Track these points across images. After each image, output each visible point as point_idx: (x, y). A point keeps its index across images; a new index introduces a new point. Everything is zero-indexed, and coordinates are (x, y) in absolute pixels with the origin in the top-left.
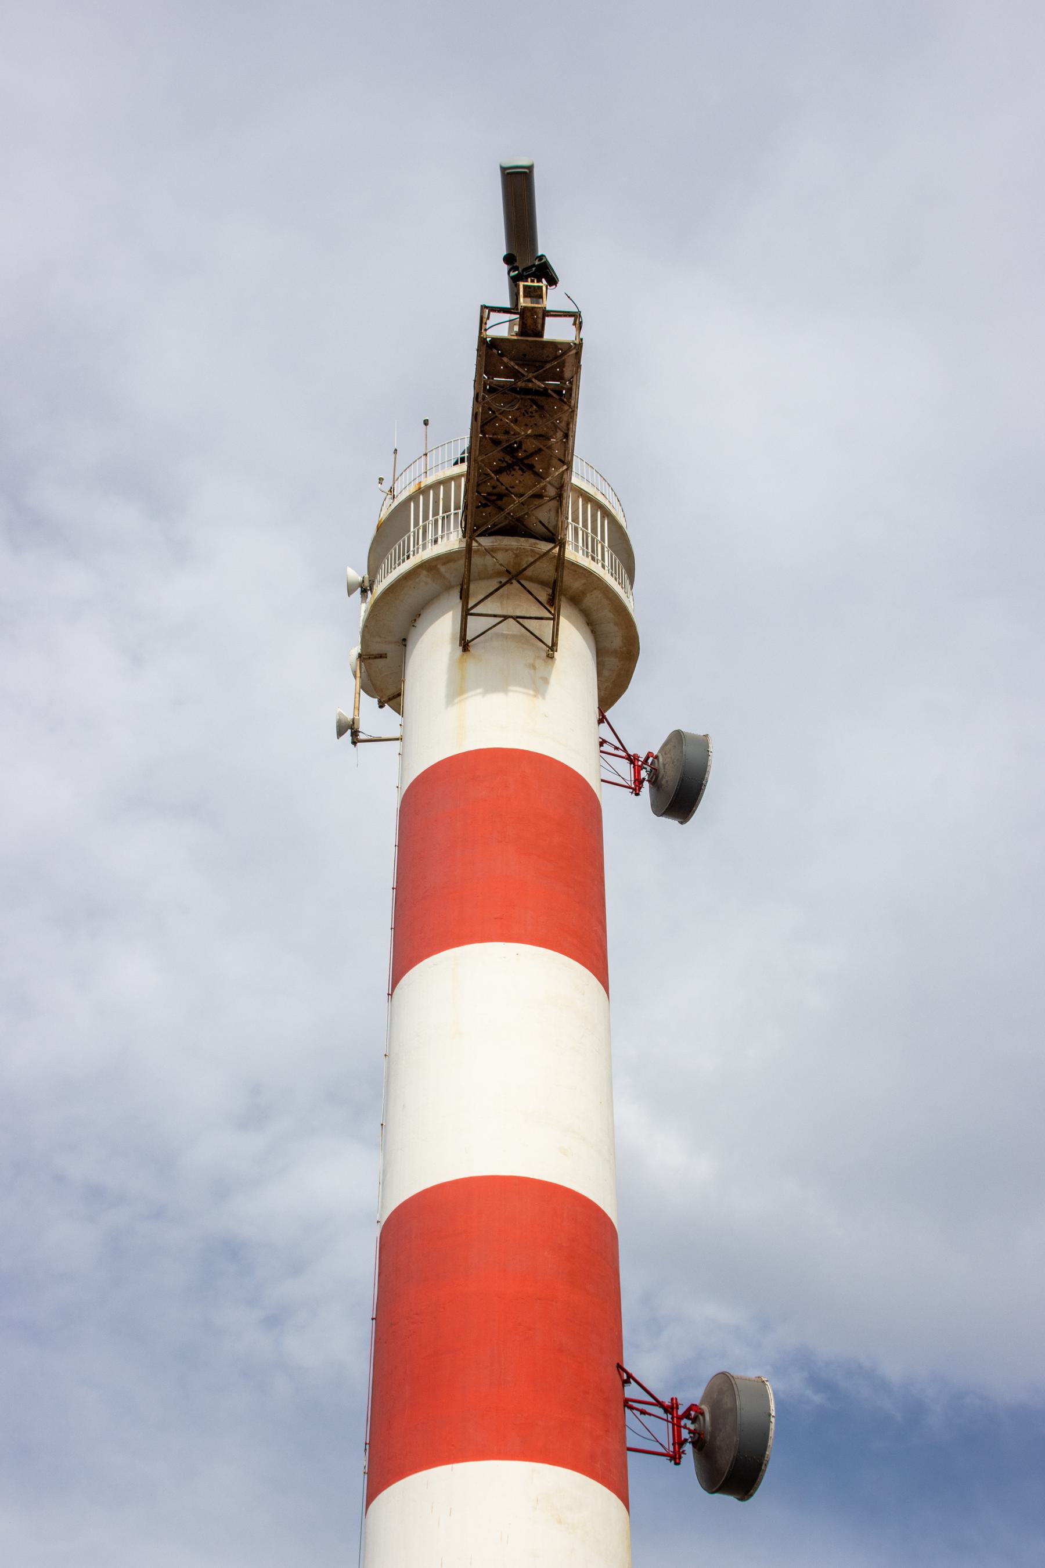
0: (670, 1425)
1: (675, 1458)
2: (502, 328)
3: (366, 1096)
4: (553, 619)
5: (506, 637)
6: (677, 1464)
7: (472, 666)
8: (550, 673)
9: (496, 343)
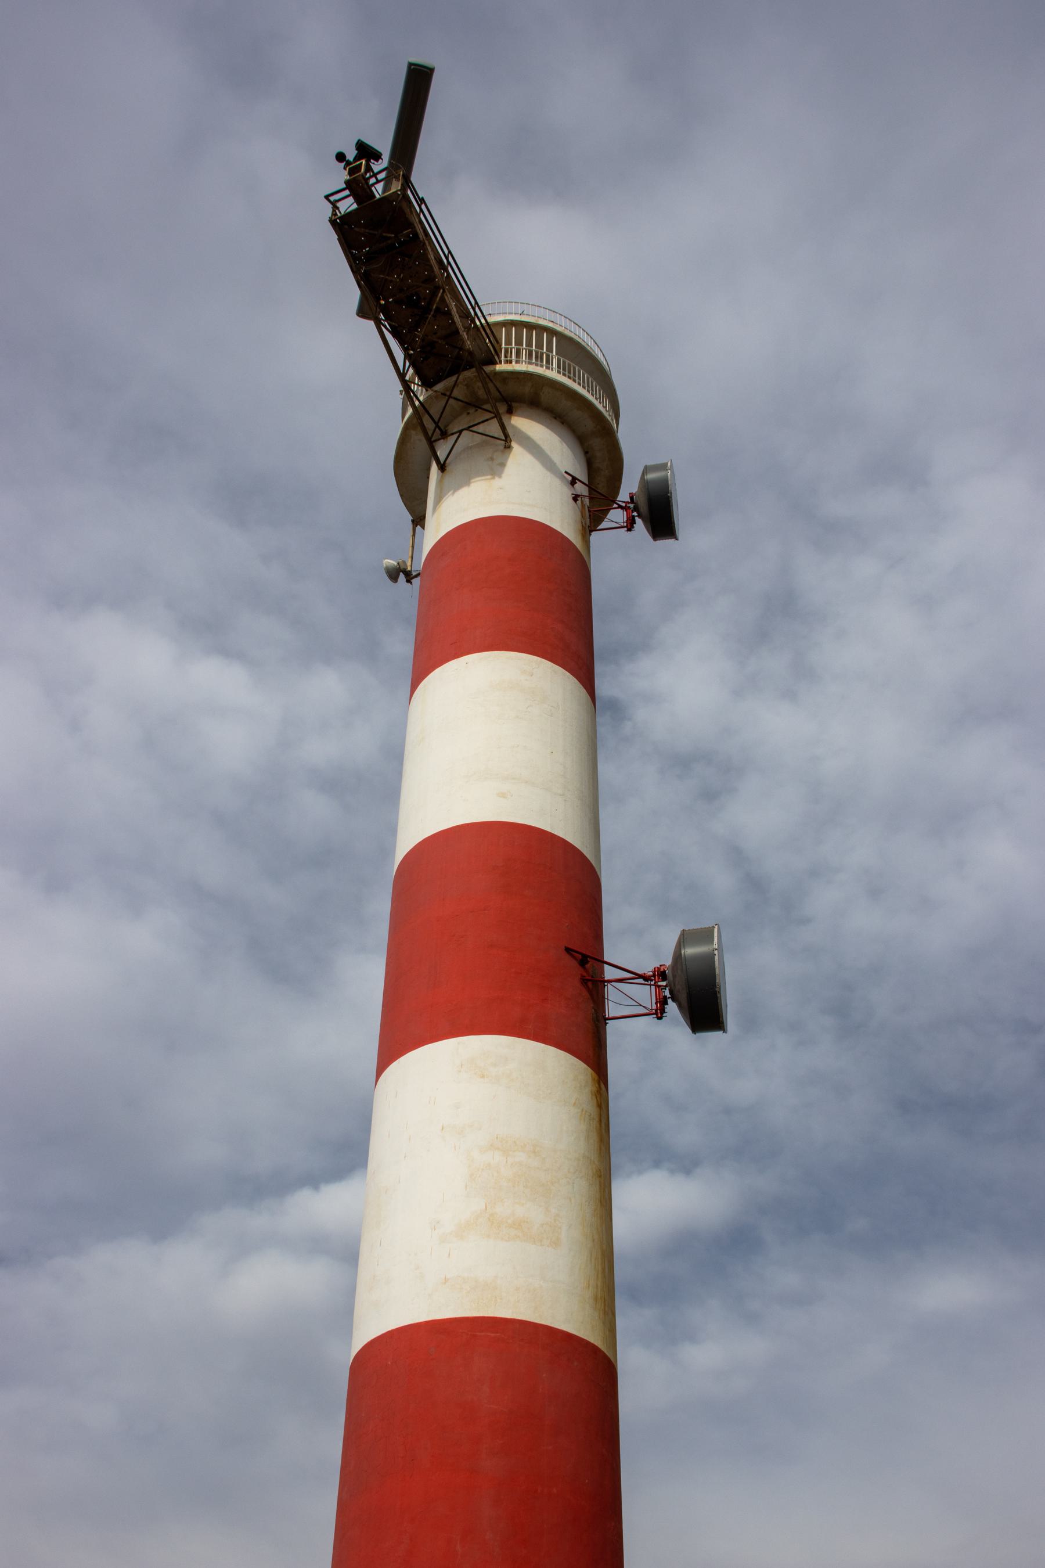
0: (653, 988)
1: (659, 1013)
2: (348, 205)
3: (380, 782)
4: (495, 417)
5: (468, 449)
6: (660, 1018)
7: (448, 477)
8: (507, 459)
9: (348, 216)
